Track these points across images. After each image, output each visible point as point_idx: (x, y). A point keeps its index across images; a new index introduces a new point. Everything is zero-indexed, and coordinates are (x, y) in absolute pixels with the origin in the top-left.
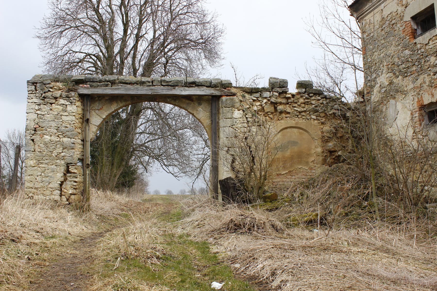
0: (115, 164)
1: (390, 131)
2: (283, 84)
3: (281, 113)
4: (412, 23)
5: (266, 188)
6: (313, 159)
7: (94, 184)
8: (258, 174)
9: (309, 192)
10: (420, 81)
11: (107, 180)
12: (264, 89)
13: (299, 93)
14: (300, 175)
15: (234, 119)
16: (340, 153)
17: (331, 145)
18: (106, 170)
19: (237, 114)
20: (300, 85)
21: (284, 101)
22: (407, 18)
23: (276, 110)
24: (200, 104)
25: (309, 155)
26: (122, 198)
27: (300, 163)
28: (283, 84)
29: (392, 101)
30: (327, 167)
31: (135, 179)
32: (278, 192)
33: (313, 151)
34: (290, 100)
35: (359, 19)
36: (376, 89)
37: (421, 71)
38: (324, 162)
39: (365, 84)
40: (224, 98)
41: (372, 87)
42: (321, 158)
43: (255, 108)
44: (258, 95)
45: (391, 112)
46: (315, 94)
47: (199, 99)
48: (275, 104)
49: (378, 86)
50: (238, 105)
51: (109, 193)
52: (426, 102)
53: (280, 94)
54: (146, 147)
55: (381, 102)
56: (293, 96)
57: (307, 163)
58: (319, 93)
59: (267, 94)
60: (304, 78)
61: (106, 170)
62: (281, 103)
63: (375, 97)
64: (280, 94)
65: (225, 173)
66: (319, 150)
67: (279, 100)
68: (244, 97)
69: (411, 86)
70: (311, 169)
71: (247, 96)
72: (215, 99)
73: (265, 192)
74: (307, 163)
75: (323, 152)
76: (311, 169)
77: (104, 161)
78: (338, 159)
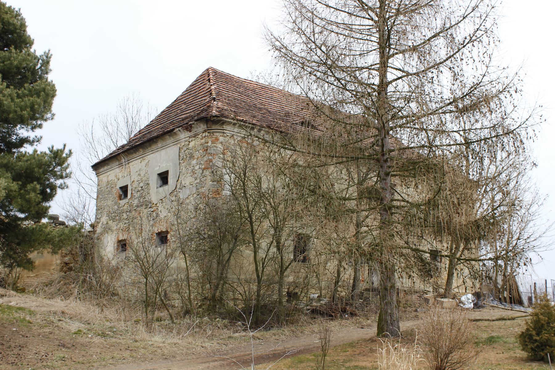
1: (103, 253)
4: (120, 191)
5: (18, 285)
6: (53, 267)
8: (14, 276)
9: (46, 289)
10: (119, 226)
14: (43, 278)
16: (72, 265)
17: (66, 259)
22: (118, 187)
25: (51, 265)
27: (44, 269)
29: (106, 234)
30: (63, 274)
32: (26, 288)
33: (54, 263)
35: (98, 175)
36: (100, 225)
37: (120, 220)
38: (61, 270)
39: (95, 221)
41: (98, 223)
42: (59, 268)
45: (105, 241)
46: (60, 224)
49: (101, 223)
52: (120, 239)
55: (102, 234)
57: (49, 270)
63: (99, 230)
66: (59, 262)
69: (115, 228)
70: (52, 274)
73: (17, 287)
74: (49, 270)
75: (61, 263)
76: (52, 274)
78: (70, 269)
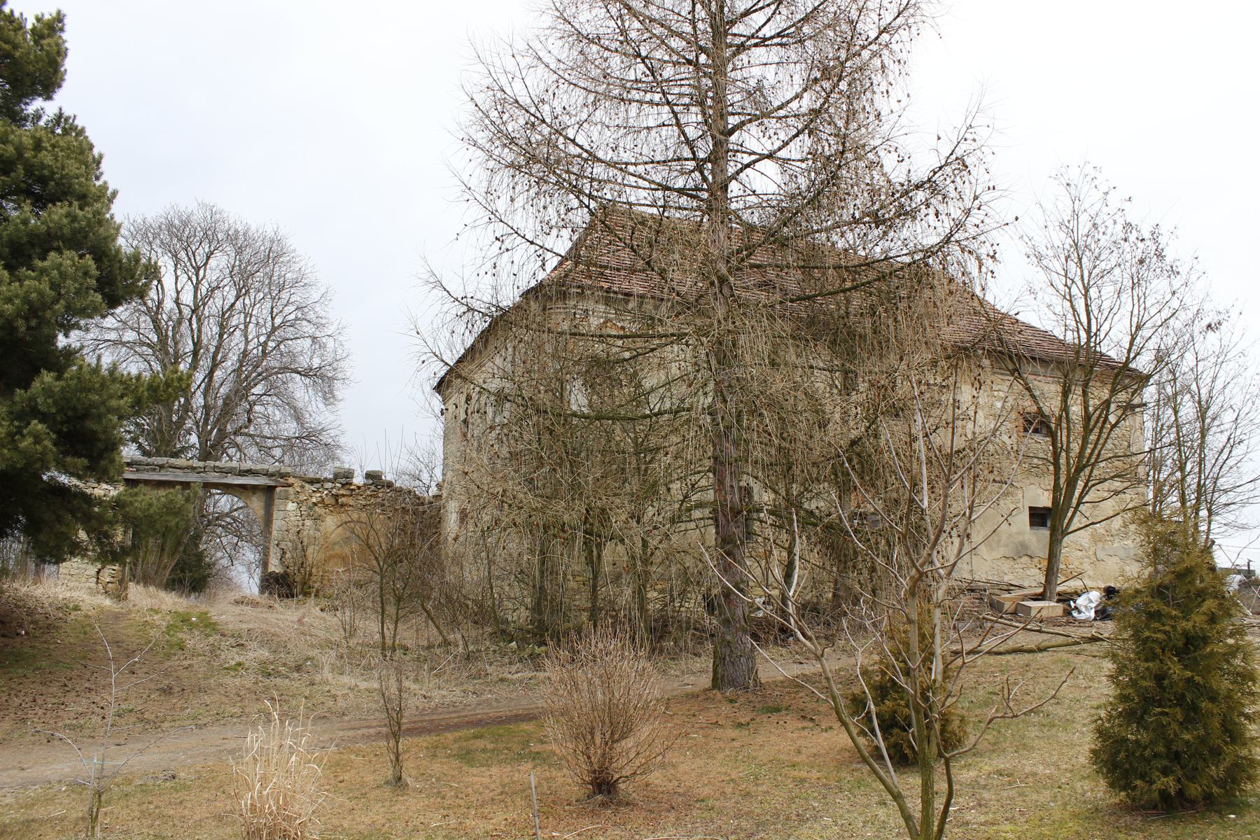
0: (167, 549)
2: (349, 475)
3: (342, 505)
7: (133, 577)
11: (152, 573)
12: (327, 480)
13: (365, 485)
15: (288, 511)
18: (152, 558)
19: (291, 506)
20: (369, 475)
21: (348, 493)
23: (337, 504)
24: (254, 493)
26: (171, 601)
28: (349, 475)
31: (209, 576)
34: (354, 492)
40: (278, 489)
43: (314, 500)
44: (318, 485)
47: (254, 489)
48: (336, 497)
50: (292, 497)
51: (152, 589)
53: (343, 485)
54: (234, 519)
56: (359, 488)
58: (390, 485)
59: (329, 485)
60: (373, 467)
61: (152, 558)
62: (343, 495)
64: (343, 485)
65: (275, 566)
67: (341, 492)
68: (303, 487)
71: (307, 486)
72: (269, 490)
77: (150, 544)
